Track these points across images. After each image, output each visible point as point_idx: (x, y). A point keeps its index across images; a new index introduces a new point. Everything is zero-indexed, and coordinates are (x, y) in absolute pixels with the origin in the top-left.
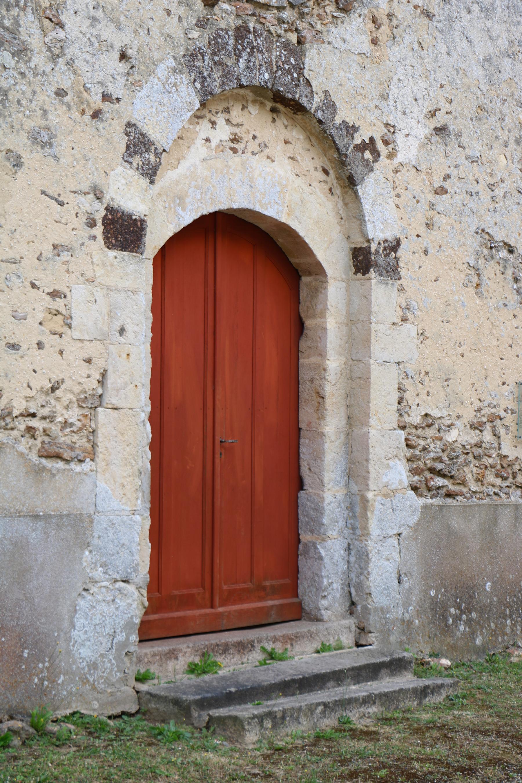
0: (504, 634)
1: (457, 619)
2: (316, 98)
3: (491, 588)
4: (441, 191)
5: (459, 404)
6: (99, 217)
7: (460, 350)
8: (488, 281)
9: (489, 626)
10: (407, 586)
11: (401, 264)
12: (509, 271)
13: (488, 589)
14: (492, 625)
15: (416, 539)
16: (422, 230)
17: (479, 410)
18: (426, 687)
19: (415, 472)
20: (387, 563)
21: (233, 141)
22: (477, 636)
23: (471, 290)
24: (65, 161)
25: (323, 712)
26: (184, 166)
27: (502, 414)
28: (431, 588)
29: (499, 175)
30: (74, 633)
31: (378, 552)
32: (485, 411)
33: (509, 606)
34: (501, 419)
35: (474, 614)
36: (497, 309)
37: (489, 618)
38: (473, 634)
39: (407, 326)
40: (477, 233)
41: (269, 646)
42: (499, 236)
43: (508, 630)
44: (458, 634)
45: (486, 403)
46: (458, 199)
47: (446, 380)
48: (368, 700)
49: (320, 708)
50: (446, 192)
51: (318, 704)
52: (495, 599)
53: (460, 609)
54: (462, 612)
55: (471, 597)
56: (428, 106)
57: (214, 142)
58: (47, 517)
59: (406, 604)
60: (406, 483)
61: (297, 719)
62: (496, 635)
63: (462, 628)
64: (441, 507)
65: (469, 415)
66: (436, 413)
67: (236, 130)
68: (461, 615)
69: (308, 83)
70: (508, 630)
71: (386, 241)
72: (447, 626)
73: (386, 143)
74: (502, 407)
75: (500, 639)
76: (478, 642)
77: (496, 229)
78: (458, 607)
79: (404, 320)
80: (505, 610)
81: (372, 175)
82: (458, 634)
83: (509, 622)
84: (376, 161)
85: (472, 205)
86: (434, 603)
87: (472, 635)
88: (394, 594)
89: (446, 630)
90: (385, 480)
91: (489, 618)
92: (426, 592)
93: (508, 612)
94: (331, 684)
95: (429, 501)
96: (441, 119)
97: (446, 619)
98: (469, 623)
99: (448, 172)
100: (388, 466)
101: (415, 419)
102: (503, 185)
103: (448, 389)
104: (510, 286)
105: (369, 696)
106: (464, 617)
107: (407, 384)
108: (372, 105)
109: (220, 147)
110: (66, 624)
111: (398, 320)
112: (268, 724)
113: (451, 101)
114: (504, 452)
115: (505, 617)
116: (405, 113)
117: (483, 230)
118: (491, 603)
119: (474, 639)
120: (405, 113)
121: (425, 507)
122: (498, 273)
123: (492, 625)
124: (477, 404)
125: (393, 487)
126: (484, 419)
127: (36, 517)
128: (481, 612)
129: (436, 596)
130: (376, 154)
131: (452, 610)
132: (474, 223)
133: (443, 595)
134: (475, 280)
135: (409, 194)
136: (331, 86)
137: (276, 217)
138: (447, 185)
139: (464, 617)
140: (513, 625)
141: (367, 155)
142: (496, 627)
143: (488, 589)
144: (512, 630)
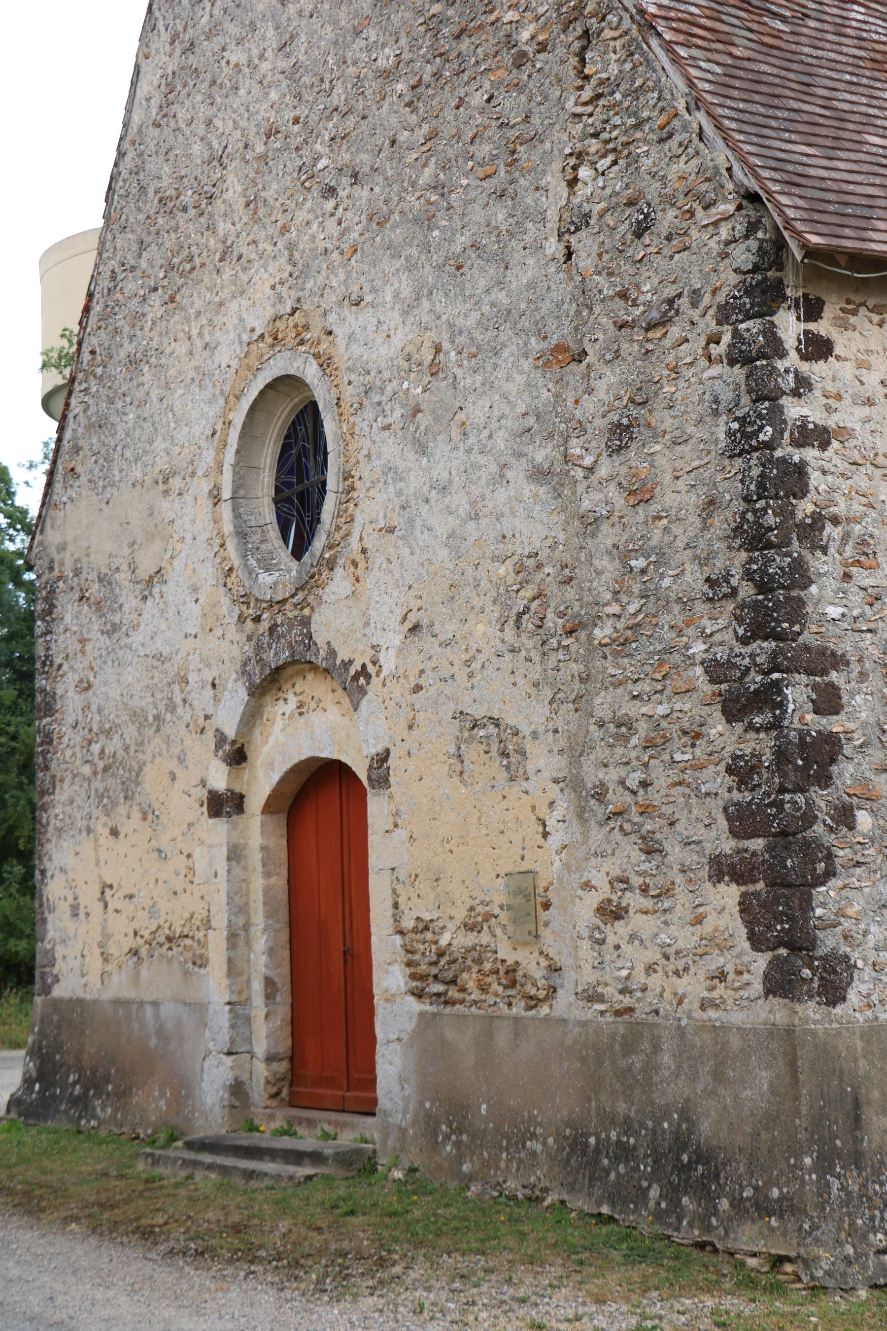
0: (498, 1168)
1: (447, 1137)
2: (322, 652)
3: (487, 1111)
4: (418, 688)
5: (449, 904)
6: (205, 799)
7: (448, 846)
8: (471, 766)
9: (481, 1154)
10: (407, 1093)
11: (391, 772)
12: (494, 748)
13: (483, 1112)
14: (485, 1154)
15: (412, 1046)
16: (405, 733)
17: (472, 909)
18: (253, 1172)
19: (413, 977)
20: (390, 1067)
21: (298, 707)
22: (465, 1162)
23: (456, 779)
24: (191, 767)
25: (182, 1165)
26: (272, 740)
27: (497, 911)
28: (427, 1099)
29: (475, 646)
30: (203, 1085)
31: (383, 1055)
32: (480, 909)
33: (506, 1136)
34: (496, 917)
35: (464, 1137)
36: (484, 793)
37: (481, 1145)
38: (461, 1158)
39: (398, 831)
40: (455, 718)
41: (327, 1128)
42: (479, 712)
43: (503, 1165)
44: (444, 1155)
45: (477, 901)
46: (432, 691)
47: (437, 880)
48: (210, 1167)
49: (180, 1162)
50: (422, 688)
51: (179, 1158)
52: (491, 1125)
53: (451, 1127)
54: (453, 1132)
55: (463, 1117)
56: (400, 612)
57: (287, 713)
58: (190, 1004)
59: (405, 1112)
60: (403, 989)
61: (166, 1164)
62: (489, 1167)
63: (449, 1148)
64: (435, 1015)
65: (461, 914)
66: (427, 916)
67: (300, 698)
68: (451, 1134)
69: (316, 644)
70: (503, 1165)
71: (378, 755)
72: (436, 1142)
73: (374, 663)
74: (497, 903)
75: (492, 1172)
76: (466, 1168)
77: (475, 706)
78: (450, 1126)
79: (396, 826)
80: (501, 1140)
81: (366, 697)
82: (444, 1155)
83: (504, 1155)
84: (368, 683)
85: (447, 691)
86: (428, 1115)
87: (459, 1159)
88: (396, 1099)
89: (435, 1146)
90: (385, 985)
91: (481, 1145)
92: (421, 1103)
93: (505, 1143)
94: (267, 1158)
95: (428, 1008)
96: (412, 618)
97: (436, 1135)
98: (458, 1144)
99: (422, 667)
100: (387, 972)
101: (408, 923)
102: (481, 655)
103: (438, 890)
104: (497, 764)
105: (213, 1164)
106: (454, 1137)
107: (400, 888)
108: (359, 636)
109: (291, 717)
110: (198, 1078)
111: (391, 827)
112: (150, 1161)
113: (421, 597)
114: (500, 956)
115: (501, 1148)
116: (384, 629)
117: (461, 713)
118: (486, 1128)
119: (461, 1164)
120: (384, 629)
121: (421, 1015)
122: (482, 753)
123: (485, 1154)
124: (470, 902)
125: (393, 992)
126: (480, 919)
127: (185, 1004)
128: (474, 1136)
129: (431, 1108)
130: (368, 677)
131: (444, 1127)
132: (449, 708)
133: (437, 1109)
134: (459, 768)
135: (393, 703)
136: (330, 637)
137: (330, 756)
138: (421, 682)
139: (454, 1137)
140: (509, 1161)
141: (362, 681)
142: (490, 1156)
143: (483, 1112)
144: (507, 1166)
